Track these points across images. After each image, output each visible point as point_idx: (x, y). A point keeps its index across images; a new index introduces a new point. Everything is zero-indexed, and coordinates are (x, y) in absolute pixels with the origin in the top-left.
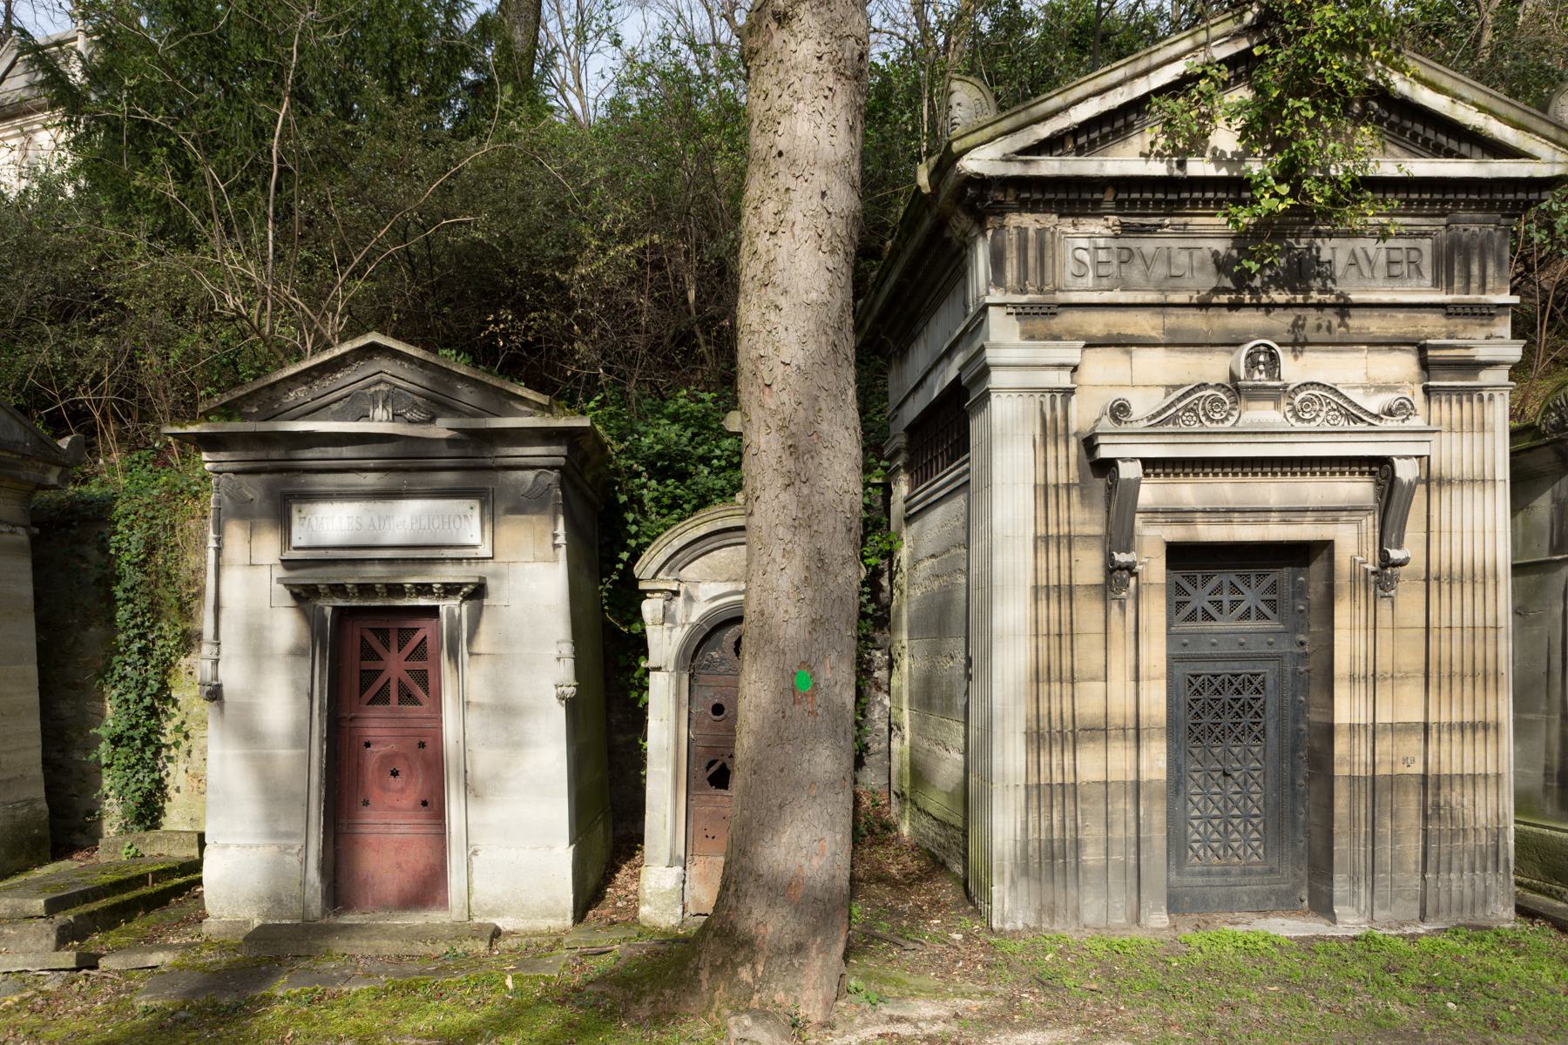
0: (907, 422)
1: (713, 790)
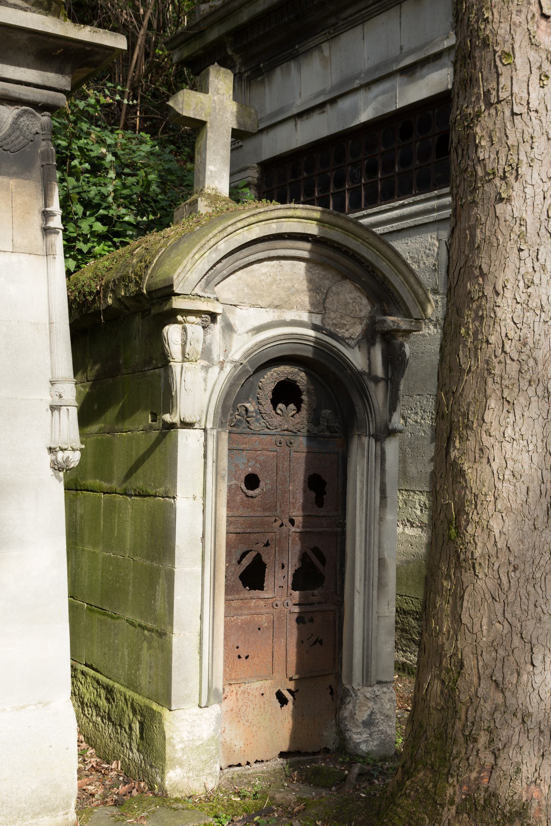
0: (267, 154)
1: (247, 593)
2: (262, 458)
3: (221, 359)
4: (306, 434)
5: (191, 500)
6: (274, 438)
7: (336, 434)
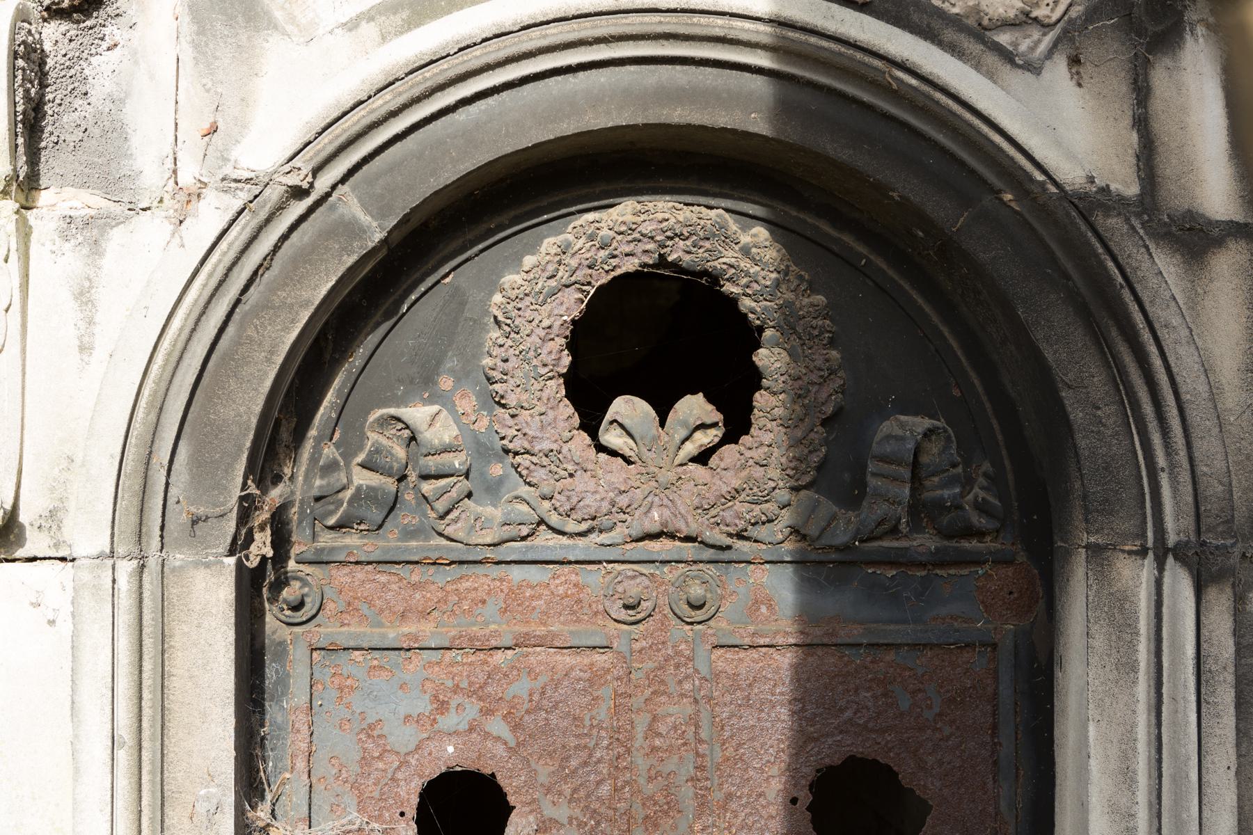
2: (521, 688)
3: (187, 178)
4: (788, 548)
6: (594, 578)
7: (972, 545)
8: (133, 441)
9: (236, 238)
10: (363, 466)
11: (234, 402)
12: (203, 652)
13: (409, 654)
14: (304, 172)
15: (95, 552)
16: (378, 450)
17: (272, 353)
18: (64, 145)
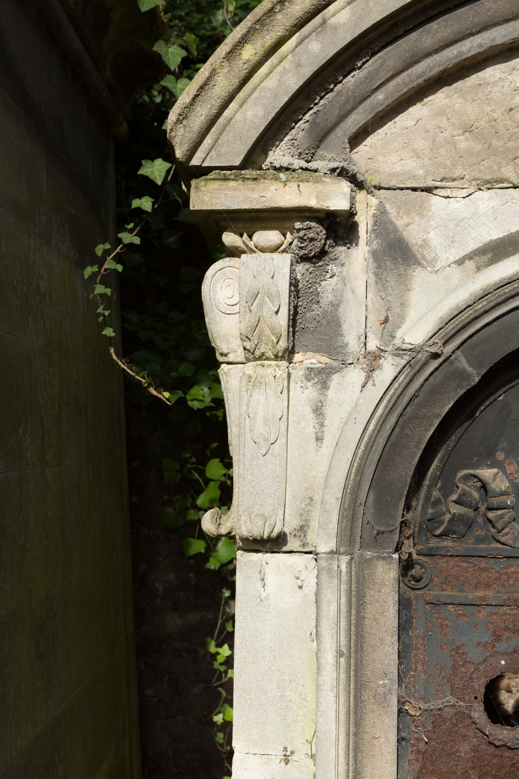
3: (373, 345)
5: (276, 765)
8: (348, 491)
9: (403, 381)
10: (455, 502)
11: (399, 469)
12: (382, 606)
13: (480, 608)
14: (440, 344)
15: (328, 550)
16: (464, 493)
17: (419, 443)
18: (307, 329)
